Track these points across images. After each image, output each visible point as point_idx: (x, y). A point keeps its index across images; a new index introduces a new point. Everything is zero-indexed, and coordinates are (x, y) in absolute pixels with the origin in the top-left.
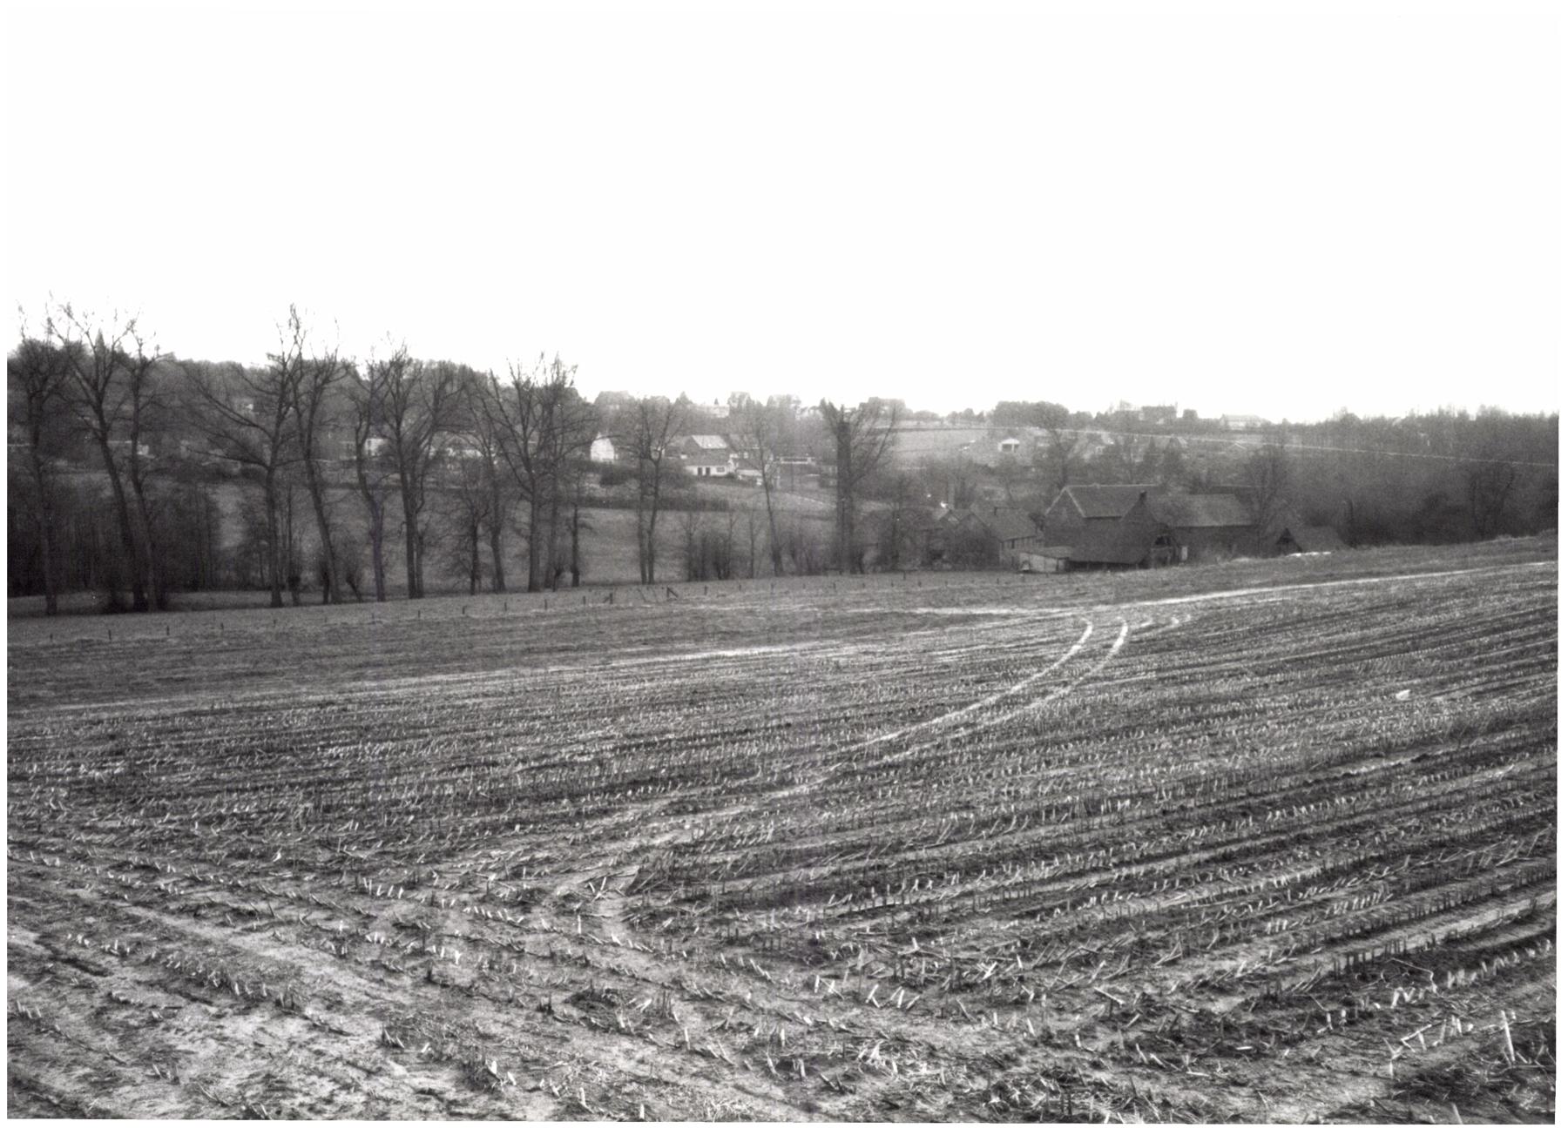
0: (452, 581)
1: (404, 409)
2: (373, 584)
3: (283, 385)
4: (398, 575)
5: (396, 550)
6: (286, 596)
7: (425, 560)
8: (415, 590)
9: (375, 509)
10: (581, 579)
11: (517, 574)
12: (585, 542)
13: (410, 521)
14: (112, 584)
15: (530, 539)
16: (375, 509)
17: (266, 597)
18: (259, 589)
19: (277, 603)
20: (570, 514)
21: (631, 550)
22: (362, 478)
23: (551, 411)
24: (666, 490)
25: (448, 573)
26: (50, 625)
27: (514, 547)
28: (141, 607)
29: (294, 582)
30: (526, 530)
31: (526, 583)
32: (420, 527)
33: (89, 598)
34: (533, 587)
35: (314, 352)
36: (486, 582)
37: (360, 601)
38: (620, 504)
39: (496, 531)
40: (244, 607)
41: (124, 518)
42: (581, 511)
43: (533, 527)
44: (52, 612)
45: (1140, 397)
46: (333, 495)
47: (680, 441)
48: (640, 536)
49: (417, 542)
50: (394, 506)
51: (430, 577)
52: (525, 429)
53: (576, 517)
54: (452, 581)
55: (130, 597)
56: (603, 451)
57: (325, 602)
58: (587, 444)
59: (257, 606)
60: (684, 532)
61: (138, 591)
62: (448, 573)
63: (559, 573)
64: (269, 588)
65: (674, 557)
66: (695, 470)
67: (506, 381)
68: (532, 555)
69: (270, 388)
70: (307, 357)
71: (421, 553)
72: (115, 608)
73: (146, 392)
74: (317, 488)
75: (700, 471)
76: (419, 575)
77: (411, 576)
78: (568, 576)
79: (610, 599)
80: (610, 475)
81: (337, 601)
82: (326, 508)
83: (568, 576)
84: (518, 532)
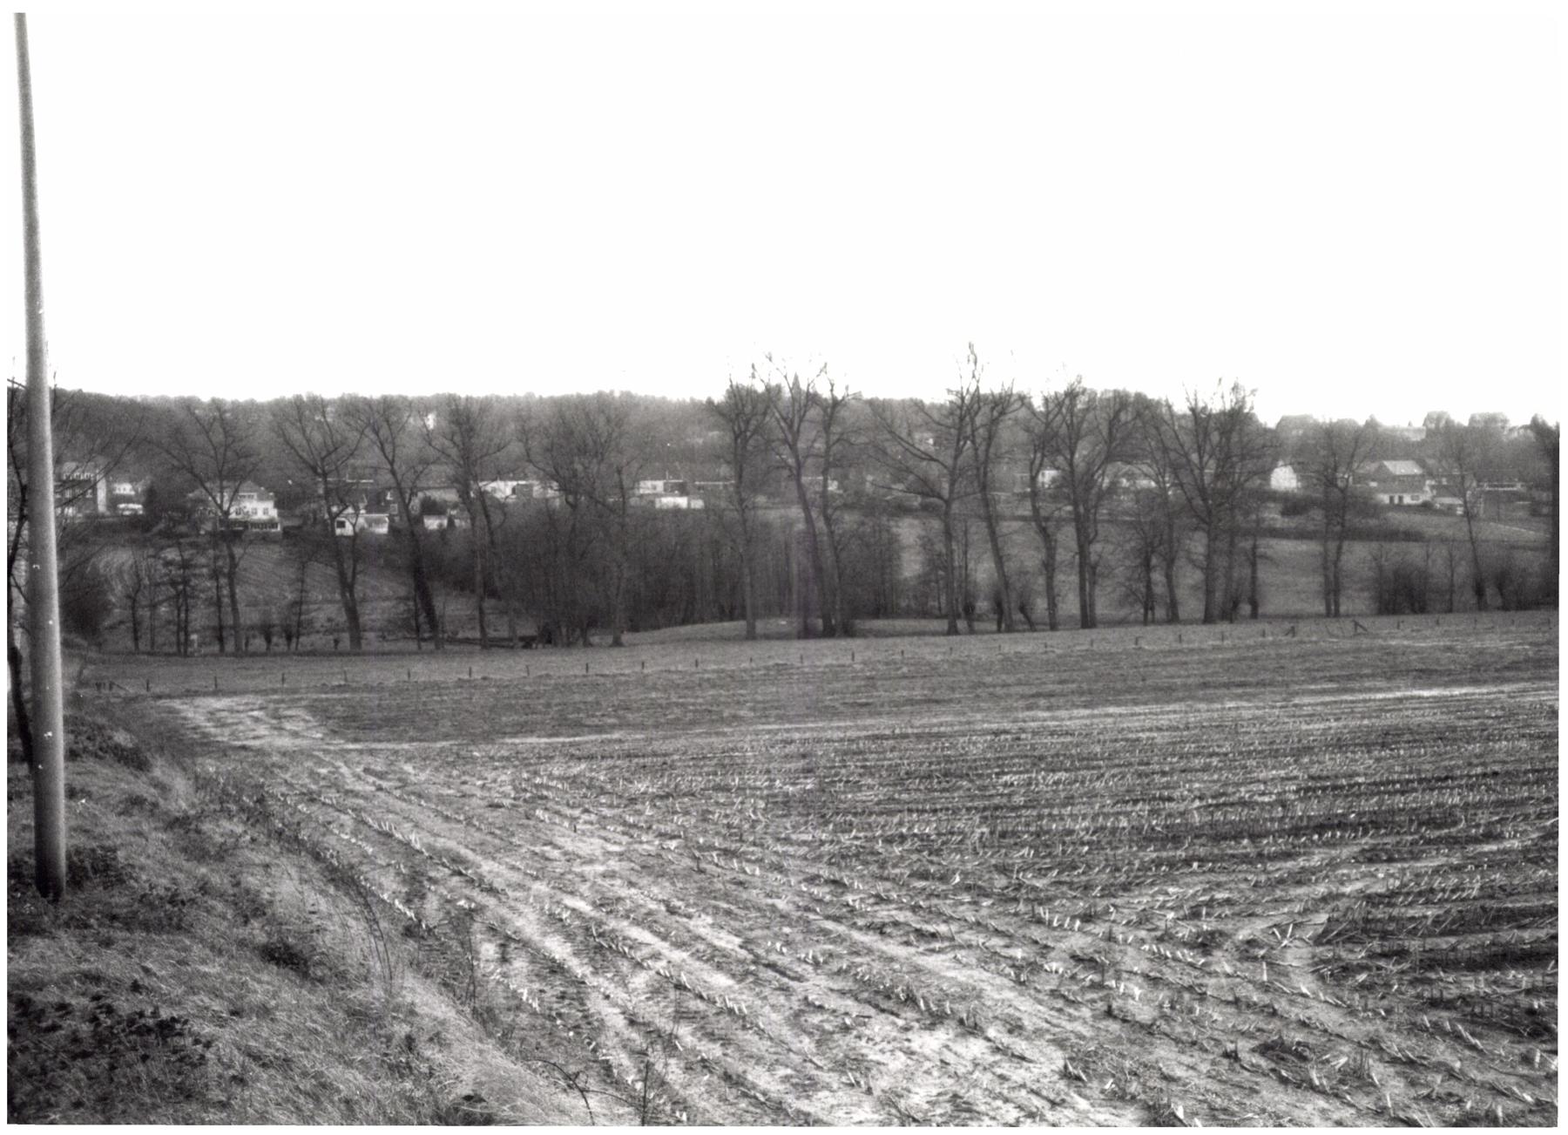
3: (962, 419)
4: (1070, 605)
5: (1067, 581)
7: (1097, 591)
8: (1087, 620)
10: (1260, 611)
11: (1191, 605)
12: (1265, 574)
13: (1083, 552)
17: (943, 625)
19: (952, 631)
20: (1246, 544)
21: (1315, 582)
22: (1036, 510)
23: (1229, 436)
24: (1353, 520)
25: (1121, 603)
27: (1189, 577)
29: (969, 610)
31: (1200, 615)
32: (1093, 558)
34: (1208, 619)
36: (1160, 612)
38: (1301, 535)
42: (1262, 542)
43: (1208, 557)
44: (751, 636)
46: (1005, 527)
49: (1088, 571)
50: (1067, 537)
51: (1102, 609)
52: (1201, 458)
53: (1255, 547)
54: (1122, 613)
56: (1284, 479)
57: (999, 631)
58: (1266, 473)
59: (934, 634)
65: (1362, 590)
67: (1181, 408)
69: (949, 422)
71: (1094, 583)
73: (836, 429)
75: (1392, 499)
76: (1092, 605)
77: (1083, 607)
79: (1293, 631)
80: (1292, 505)
81: (1010, 630)
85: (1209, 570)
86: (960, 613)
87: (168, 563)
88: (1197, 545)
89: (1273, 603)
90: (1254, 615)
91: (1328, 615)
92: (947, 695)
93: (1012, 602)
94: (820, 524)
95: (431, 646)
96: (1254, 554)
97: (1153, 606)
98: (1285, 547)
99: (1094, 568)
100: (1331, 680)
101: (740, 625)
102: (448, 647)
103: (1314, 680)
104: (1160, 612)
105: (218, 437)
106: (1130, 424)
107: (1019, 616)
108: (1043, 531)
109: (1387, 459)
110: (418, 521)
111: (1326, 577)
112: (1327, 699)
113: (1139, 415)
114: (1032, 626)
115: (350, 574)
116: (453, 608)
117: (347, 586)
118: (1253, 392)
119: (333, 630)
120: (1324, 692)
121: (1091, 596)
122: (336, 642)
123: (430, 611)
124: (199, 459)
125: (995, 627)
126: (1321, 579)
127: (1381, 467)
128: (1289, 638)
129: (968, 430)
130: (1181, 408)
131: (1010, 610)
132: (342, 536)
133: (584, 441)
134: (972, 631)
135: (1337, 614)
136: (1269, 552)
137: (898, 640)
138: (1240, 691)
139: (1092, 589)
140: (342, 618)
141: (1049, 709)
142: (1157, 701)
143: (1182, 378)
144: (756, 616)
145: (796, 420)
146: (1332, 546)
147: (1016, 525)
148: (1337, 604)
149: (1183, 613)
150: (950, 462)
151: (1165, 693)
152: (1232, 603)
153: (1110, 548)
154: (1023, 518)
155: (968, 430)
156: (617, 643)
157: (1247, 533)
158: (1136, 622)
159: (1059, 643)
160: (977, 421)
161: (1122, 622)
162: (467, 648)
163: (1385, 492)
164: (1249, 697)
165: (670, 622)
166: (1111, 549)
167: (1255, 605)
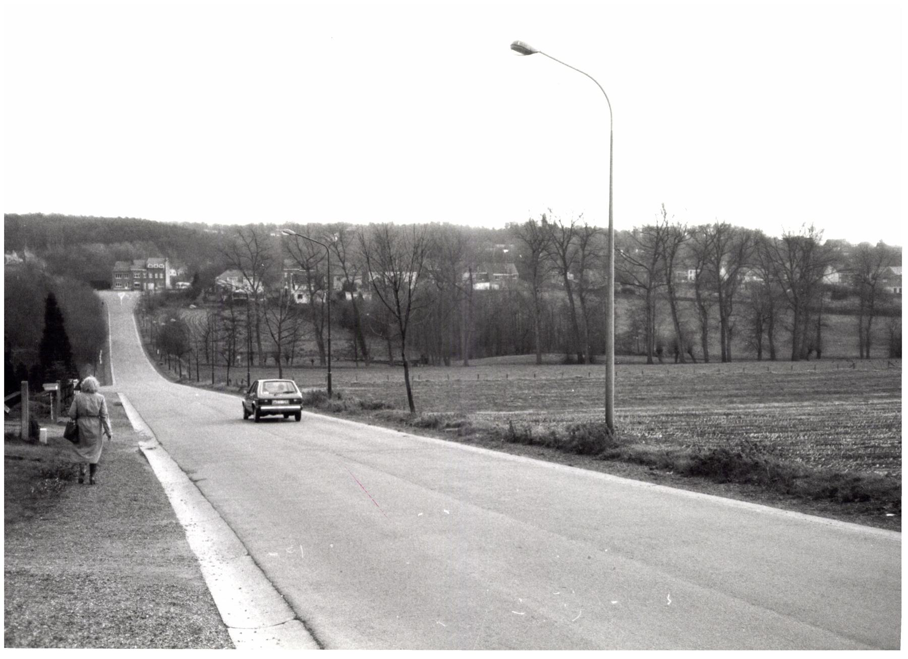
0: (746, 354)
1: (722, 255)
2: (702, 354)
3: (657, 243)
4: (715, 350)
5: (715, 337)
6: (654, 359)
7: (732, 343)
8: (725, 358)
9: (704, 312)
10: (822, 355)
11: (785, 351)
12: (826, 335)
13: (724, 321)
14: (565, 349)
15: (794, 332)
16: (704, 312)
17: (645, 359)
18: (636, 355)
19: (650, 362)
20: (816, 317)
21: (855, 339)
22: (698, 295)
23: (804, 253)
24: (877, 303)
25: (745, 349)
26: (537, 370)
27: (783, 337)
28: (581, 362)
29: (660, 351)
30: (791, 327)
31: (790, 357)
32: (730, 324)
33: (552, 357)
34: (794, 359)
35: (672, 222)
36: (765, 354)
37: (695, 362)
38: (844, 312)
39: (771, 327)
40: (634, 363)
41: (573, 316)
42: (824, 316)
43: (795, 325)
44: (539, 363)
45: (269, 223)
46: (681, 305)
47: (882, 270)
48: (860, 331)
49: (727, 332)
50: (715, 312)
51: (734, 352)
52: (791, 266)
53: (819, 319)
54: (746, 354)
55: (576, 357)
56: (832, 277)
57: (676, 363)
58: (821, 274)
59: (639, 363)
60: (888, 330)
61: (580, 355)
62: (745, 349)
63: (810, 351)
64: (646, 355)
65: (882, 344)
66: (892, 289)
67: (780, 238)
68: (794, 341)
69: (650, 245)
70: (618, 227)
71: (730, 339)
72: (568, 362)
73: (588, 248)
74: (673, 300)
75: (895, 290)
76: (729, 350)
77: (723, 350)
78: (815, 353)
79: (854, 366)
80: (837, 293)
81: (683, 362)
82: (678, 314)
83: (815, 353)
84: (786, 328)
85: (795, 332)
86: (655, 352)
87: (223, 318)
88: (789, 318)
89: (830, 350)
90: (819, 357)
91: (862, 357)
92: (681, 395)
93: (683, 348)
94: (577, 302)
95: (363, 364)
96: (819, 324)
97: (762, 350)
98: (834, 319)
99: (731, 330)
100: (884, 391)
101: (533, 357)
102: (371, 365)
103: (877, 391)
104: (765, 354)
105: (253, 247)
106: (745, 247)
107: (687, 355)
108: (702, 308)
109: (893, 265)
110: (342, 295)
111: (860, 337)
112: (888, 401)
113: (757, 243)
114: (694, 360)
115: (320, 328)
116: (376, 346)
117: (319, 333)
118: (822, 231)
119: (311, 354)
120: (881, 397)
121: (729, 345)
122: (312, 361)
123: (363, 346)
124: (243, 260)
125: (673, 360)
126: (858, 338)
127: (889, 271)
128: (851, 369)
129: (661, 249)
130: (780, 238)
131: (679, 351)
132: (300, 304)
133: (440, 250)
134: (661, 362)
135: (868, 357)
136: (828, 322)
137: (627, 366)
138: (838, 396)
139: (729, 342)
140: (317, 349)
141: (741, 403)
142: (796, 400)
143: (775, 219)
144: (542, 352)
145: (565, 244)
146: (865, 319)
147: (687, 304)
148: (868, 352)
149: (779, 355)
150: (649, 266)
151: (799, 396)
152: (808, 349)
153: (738, 318)
154: (691, 300)
155: (661, 249)
156: (466, 365)
157: (813, 310)
158: (752, 360)
159: (704, 370)
160: (662, 243)
161: (742, 360)
162: (378, 365)
163: (890, 285)
164: (847, 399)
165: (490, 355)
166: (740, 320)
167: (819, 352)
